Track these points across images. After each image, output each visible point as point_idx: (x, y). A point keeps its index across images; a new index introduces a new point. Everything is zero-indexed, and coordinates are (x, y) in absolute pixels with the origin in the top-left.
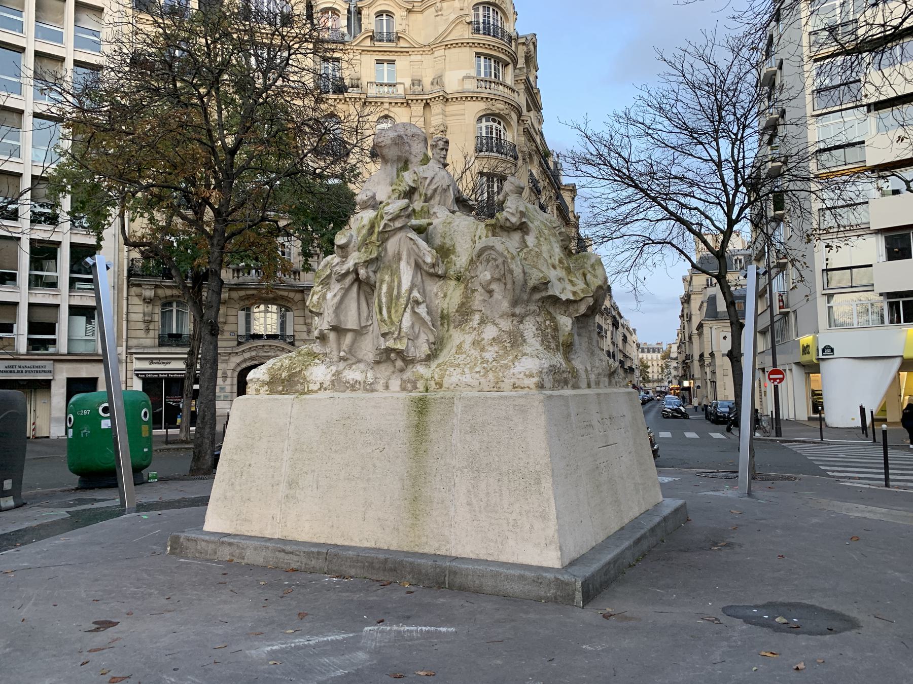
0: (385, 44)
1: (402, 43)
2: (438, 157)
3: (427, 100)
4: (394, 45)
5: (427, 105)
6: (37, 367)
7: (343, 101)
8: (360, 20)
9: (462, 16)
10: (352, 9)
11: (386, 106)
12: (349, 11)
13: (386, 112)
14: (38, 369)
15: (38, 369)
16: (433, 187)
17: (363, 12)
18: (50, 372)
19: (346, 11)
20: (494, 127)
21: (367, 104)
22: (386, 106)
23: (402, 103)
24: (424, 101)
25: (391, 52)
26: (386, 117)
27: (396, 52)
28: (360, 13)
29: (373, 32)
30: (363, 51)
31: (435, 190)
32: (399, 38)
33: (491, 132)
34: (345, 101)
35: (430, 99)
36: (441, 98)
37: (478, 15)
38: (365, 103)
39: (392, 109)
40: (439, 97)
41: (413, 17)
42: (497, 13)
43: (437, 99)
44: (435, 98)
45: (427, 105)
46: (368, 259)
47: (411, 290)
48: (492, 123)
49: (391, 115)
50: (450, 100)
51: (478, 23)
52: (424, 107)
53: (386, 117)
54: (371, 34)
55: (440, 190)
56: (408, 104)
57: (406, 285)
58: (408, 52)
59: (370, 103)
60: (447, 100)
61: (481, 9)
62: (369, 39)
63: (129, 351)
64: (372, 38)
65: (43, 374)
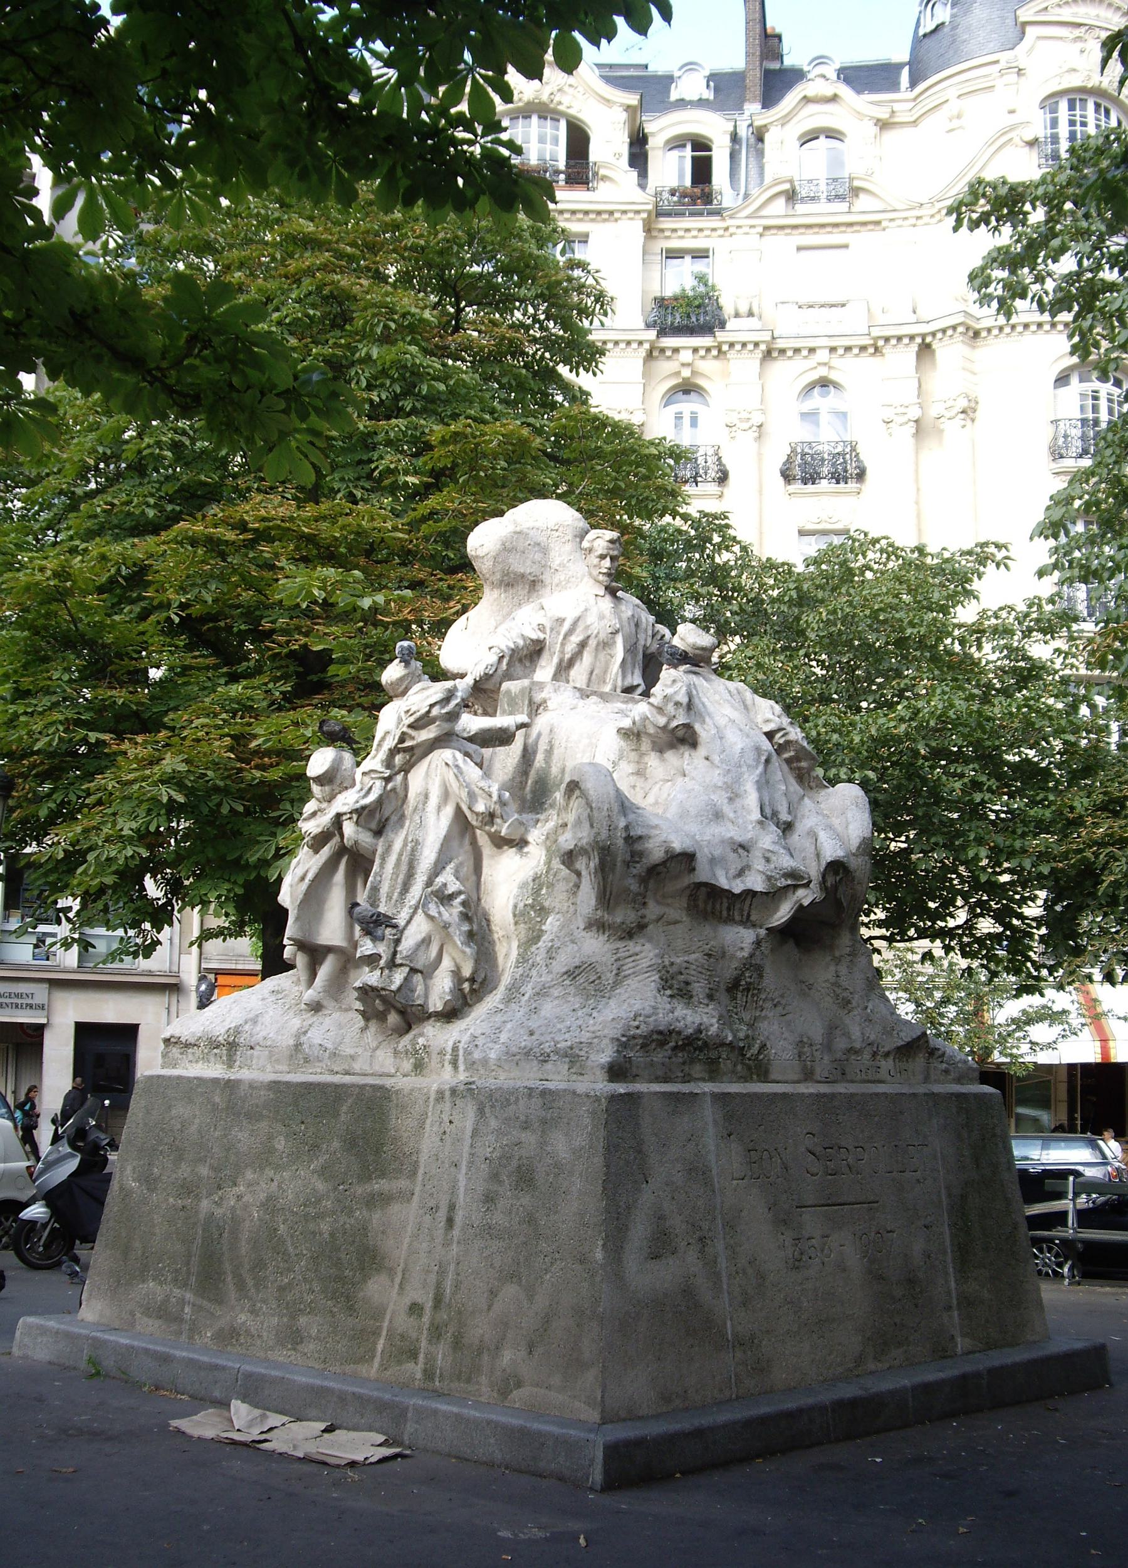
0: (823, 207)
1: (863, 202)
2: (595, 572)
3: (924, 336)
4: (843, 206)
5: (925, 349)
6: (17, 996)
7: (715, 352)
8: (760, 154)
9: (1012, 128)
10: (743, 132)
11: (822, 355)
12: (735, 138)
13: (822, 372)
14: (19, 1001)
15: (19, 1001)
16: (576, 639)
17: (768, 137)
18: (42, 1007)
19: (728, 138)
20: (1103, 396)
21: (775, 354)
22: (822, 355)
23: (863, 348)
24: (919, 340)
25: (836, 225)
26: (824, 383)
27: (851, 225)
28: (761, 139)
29: (791, 181)
30: (766, 228)
31: (583, 645)
32: (856, 191)
33: (1095, 409)
34: (720, 351)
35: (934, 334)
36: (960, 329)
37: (1054, 123)
38: (768, 354)
39: (835, 361)
40: (954, 328)
41: (890, 135)
42: (1107, 112)
43: (950, 332)
44: (944, 331)
45: (925, 349)
46: (358, 805)
47: (438, 869)
48: (1097, 385)
49: (833, 376)
50: (984, 334)
51: (1055, 139)
52: (919, 355)
53: (824, 383)
54: (787, 186)
55: (592, 643)
56: (876, 349)
57: (428, 856)
58: (878, 223)
59: (782, 351)
60: (977, 334)
61: (1063, 105)
62: (781, 201)
63: (204, 966)
64: (791, 196)
65: (29, 1012)
